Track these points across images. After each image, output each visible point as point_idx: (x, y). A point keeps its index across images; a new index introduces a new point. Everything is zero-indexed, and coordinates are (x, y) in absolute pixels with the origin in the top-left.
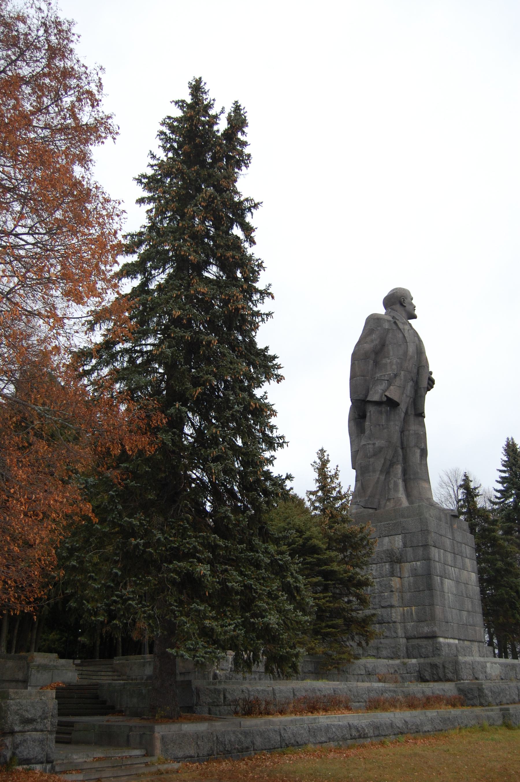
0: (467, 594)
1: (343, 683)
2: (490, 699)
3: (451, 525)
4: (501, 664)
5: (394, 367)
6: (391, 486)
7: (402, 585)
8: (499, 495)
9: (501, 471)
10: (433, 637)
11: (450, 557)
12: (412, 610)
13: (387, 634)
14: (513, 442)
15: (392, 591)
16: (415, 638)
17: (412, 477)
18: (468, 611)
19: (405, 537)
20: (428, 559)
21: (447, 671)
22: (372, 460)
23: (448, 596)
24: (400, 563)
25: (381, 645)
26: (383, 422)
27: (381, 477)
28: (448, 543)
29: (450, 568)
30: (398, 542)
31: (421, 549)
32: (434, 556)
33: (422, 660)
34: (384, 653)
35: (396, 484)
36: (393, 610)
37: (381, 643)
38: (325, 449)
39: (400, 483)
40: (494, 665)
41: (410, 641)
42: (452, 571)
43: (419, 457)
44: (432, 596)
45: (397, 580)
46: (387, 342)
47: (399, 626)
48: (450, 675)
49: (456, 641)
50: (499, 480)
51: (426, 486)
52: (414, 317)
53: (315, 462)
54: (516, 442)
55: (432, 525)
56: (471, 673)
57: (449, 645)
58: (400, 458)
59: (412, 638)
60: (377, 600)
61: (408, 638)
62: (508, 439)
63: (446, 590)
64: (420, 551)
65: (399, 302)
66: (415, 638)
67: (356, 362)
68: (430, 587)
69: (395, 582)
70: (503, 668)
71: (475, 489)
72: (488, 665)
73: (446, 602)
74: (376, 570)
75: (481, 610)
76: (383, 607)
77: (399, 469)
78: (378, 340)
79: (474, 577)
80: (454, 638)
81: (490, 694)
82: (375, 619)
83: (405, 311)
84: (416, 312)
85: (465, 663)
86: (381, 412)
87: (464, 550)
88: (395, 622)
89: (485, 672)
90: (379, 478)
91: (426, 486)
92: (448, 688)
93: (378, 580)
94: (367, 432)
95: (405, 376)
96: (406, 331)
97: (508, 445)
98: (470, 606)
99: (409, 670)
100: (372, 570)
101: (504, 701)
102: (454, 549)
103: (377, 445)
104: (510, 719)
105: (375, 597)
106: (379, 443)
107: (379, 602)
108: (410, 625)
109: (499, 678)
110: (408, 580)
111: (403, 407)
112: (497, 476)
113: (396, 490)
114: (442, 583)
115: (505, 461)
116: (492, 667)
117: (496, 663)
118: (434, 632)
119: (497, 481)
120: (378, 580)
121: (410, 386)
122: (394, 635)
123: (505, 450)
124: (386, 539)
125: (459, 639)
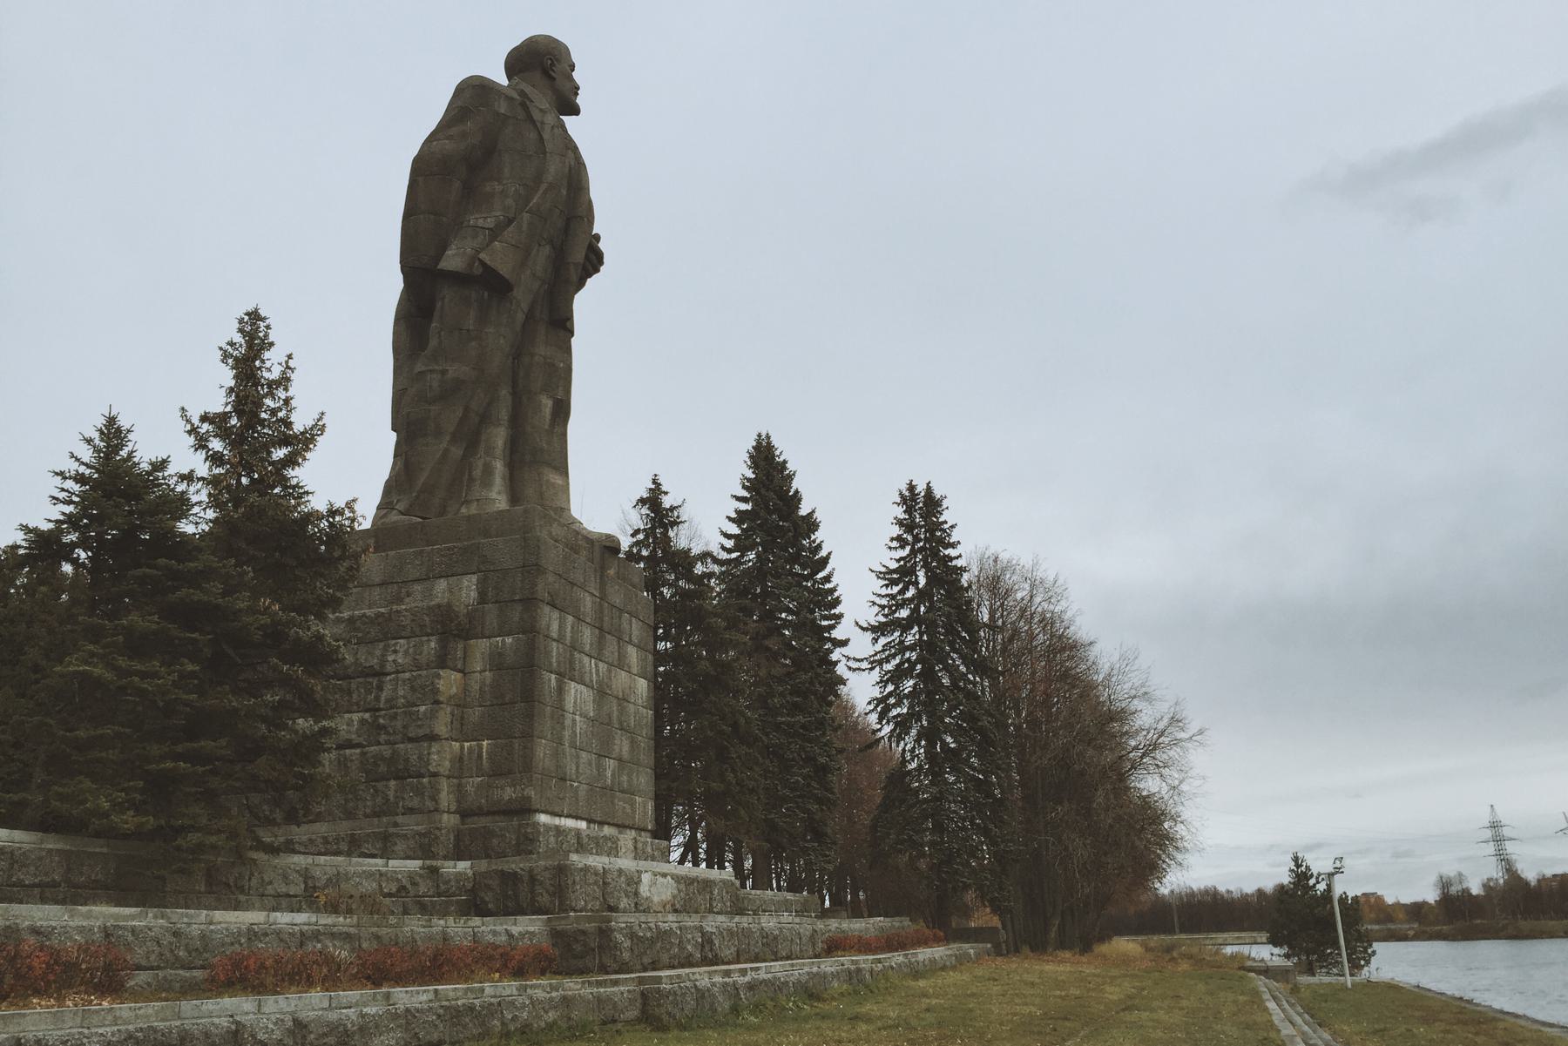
0: (621, 723)
1: (151, 913)
2: (626, 955)
3: (603, 568)
4: (677, 879)
5: (510, 201)
6: (477, 473)
7: (466, 689)
8: (730, 544)
9: (739, 499)
10: (524, 810)
11: (587, 636)
12: (480, 747)
14: (769, 443)
15: (437, 702)
16: (480, 812)
18: (620, 760)
20: (531, 631)
21: (539, 889)
23: (574, 721)
24: (467, 638)
25: (392, 830)
26: (470, 323)
27: (453, 449)
28: (588, 603)
29: (586, 659)
30: (468, 589)
31: (519, 608)
32: (549, 626)
33: (483, 865)
34: (400, 847)
35: (488, 471)
37: (396, 825)
38: (263, 313)
39: (499, 466)
40: (660, 879)
43: (548, 417)
44: (530, 716)
45: (456, 676)
47: (444, 785)
48: (544, 899)
49: (583, 825)
50: (734, 515)
51: (559, 481)
52: (574, 110)
53: (231, 344)
54: (775, 442)
55: (552, 557)
56: (598, 893)
57: (558, 830)
58: (504, 414)
60: (399, 724)
61: (464, 814)
63: (569, 706)
64: (516, 614)
65: (543, 67)
66: (480, 812)
67: (420, 179)
68: (529, 695)
69: (449, 683)
70: (682, 887)
71: (672, 509)
72: (646, 878)
73: (567, 733)
74: (406, 652)
75: (652, 762)
76: (411, 740)
77: (499, 437)
79: (642, 685)
80: (577, 818)
81: (627, 944)
82: (328, 743)
84: (580, 101)
85: (586, 869)
87: (625, 625)
88: (435, 775)
89: (636, 894)
90: (446, 451)
91: (559, 481)
92: (529, 927)
93: (407, 675)
94: (433, 343)
96: (547, 129)
97: (758, 448)
98: (626, 748)
99: (443, 887)
100: (395, 652)
101: (665, 958)
103: (450, 375)
104: (659, 1005)
105: (394, 717)
106: (455, 370)
107: (405, 727)
108: (472, 783)
109: (668, 907)
110: (481, 675)
111: (522, 296)
112: (732, 507)
113: (487, 483)
114: (561, 690)
115: (749, 480)
116: (653, 884)
117: (664, 875)
119: (729, 518)
120: (407, 675)
121: (542, 255)
122: (430, 804)
123: (751, 457)
124: (442, 585)
125: (590, 821)
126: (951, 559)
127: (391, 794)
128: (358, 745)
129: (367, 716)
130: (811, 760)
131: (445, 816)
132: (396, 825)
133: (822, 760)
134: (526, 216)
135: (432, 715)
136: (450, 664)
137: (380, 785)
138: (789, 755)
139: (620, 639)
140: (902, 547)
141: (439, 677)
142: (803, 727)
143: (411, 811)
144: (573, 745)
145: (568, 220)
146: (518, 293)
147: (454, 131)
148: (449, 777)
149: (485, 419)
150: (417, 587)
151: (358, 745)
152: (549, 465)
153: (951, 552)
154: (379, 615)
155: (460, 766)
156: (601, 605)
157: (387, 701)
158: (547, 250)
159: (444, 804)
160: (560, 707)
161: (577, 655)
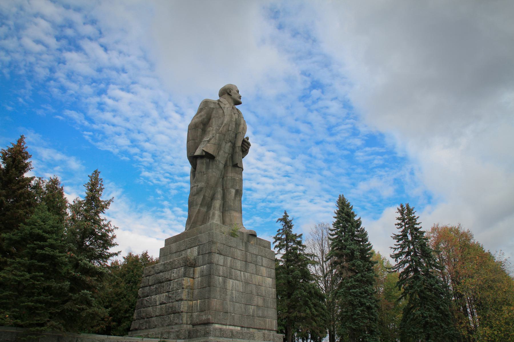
0: (257, 293)
6: (211, 215)
11: (239, 264)
13: (177, 321)
15: (183, 288)
17: (227, 209)
19: (200, 247)
20: (210, 263)
22: (195, 197)
24: (194, 267)
26: (204, 170)
28: (238, 253)
29: (239, 272)
31: (207, 255)
35: (214, 214)
36: (182, 302)
37: (172, 328)
38: (99, 171)
39: (217, 213)
41: (195, 327)
42: (241, 275)
46: (212, 117)
49: (239, 328)
58: (219, 196)
59: (196, 325)
62: (340, 196)
69: (187, 282)
76: (177, 301)
77: (217, 203)
78: (206, 115)
83: (232, 98)
86: (203, 163)
90: (199, 210)
93: (176, 280)
95: (219, 137)
97: (340, 200)
102: (247, 258)
103: (199, 187)
105: (173, 294)
110: (198, 279)
114: (224, 282)
118: (209, 319)
123: (338, 203)
125: (242, 327)
126: (419, 229)
127: (172, 318)
128: (165, 303)
129: (167, 294)
130: (362, 304)
131: (185, 326)
132: (172, 328)
133: (367, 304)
134: (217, 135)
135: (182, 292)
136: (187, 275)
137: (169, 316)
138: (355, 303)
139: (256, 265)
140: (401, 227)
141: (183, 280)
142: (361, 293)
143: (176, 324)
144: (232, 301)
145: (236, 134)
146: (218, 158)
147: (198, 116)
148: (187, 313)
149: (213, 198)
150: (184, 252)
151: (165, 303)
152: (234, 210)
153: (418, 226)
154: (171, 262)
155: (191, 310)
156: (245, 254)
157: (172, 289)
158: (229, 144)
159: (185, 321)
160: (224, 289)
161: (233, 270)
